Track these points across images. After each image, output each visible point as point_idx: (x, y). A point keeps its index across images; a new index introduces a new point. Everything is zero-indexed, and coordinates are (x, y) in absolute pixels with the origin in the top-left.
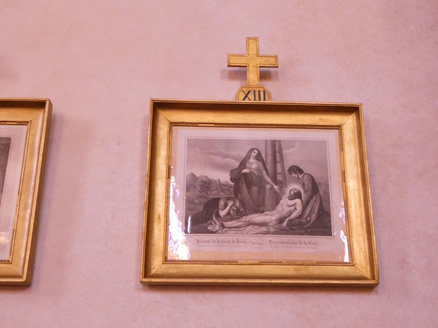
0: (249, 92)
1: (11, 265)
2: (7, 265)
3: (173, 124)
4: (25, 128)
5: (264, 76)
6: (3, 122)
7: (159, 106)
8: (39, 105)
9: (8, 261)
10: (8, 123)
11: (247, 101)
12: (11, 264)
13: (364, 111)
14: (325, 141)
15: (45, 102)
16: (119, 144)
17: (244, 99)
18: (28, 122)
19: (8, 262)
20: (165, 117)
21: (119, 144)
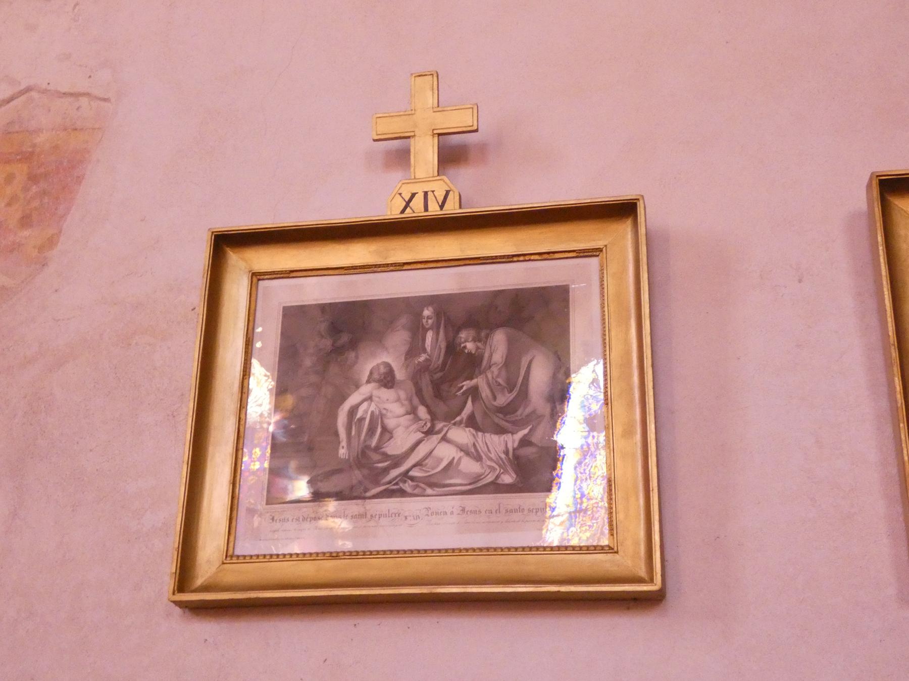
0: (413, 195)
1: (617, 557)
2: (610, 556)
3: (257, 277)
4: (594, 262)
5: (451, 155)
6: (548, 253)
7: (225, 243)
8: (625, 210)
9: (611, 548)
10: (557, 256)
11: (408, 213)
12: (617, 552)
13: (651, 213)
14: (284, 308)
15: (635, 204)
16: (800, 281)
17: (403, 212)
18: (600, 250)
19: (609, 550)
20: (241, 264)
21: (800, 281)
